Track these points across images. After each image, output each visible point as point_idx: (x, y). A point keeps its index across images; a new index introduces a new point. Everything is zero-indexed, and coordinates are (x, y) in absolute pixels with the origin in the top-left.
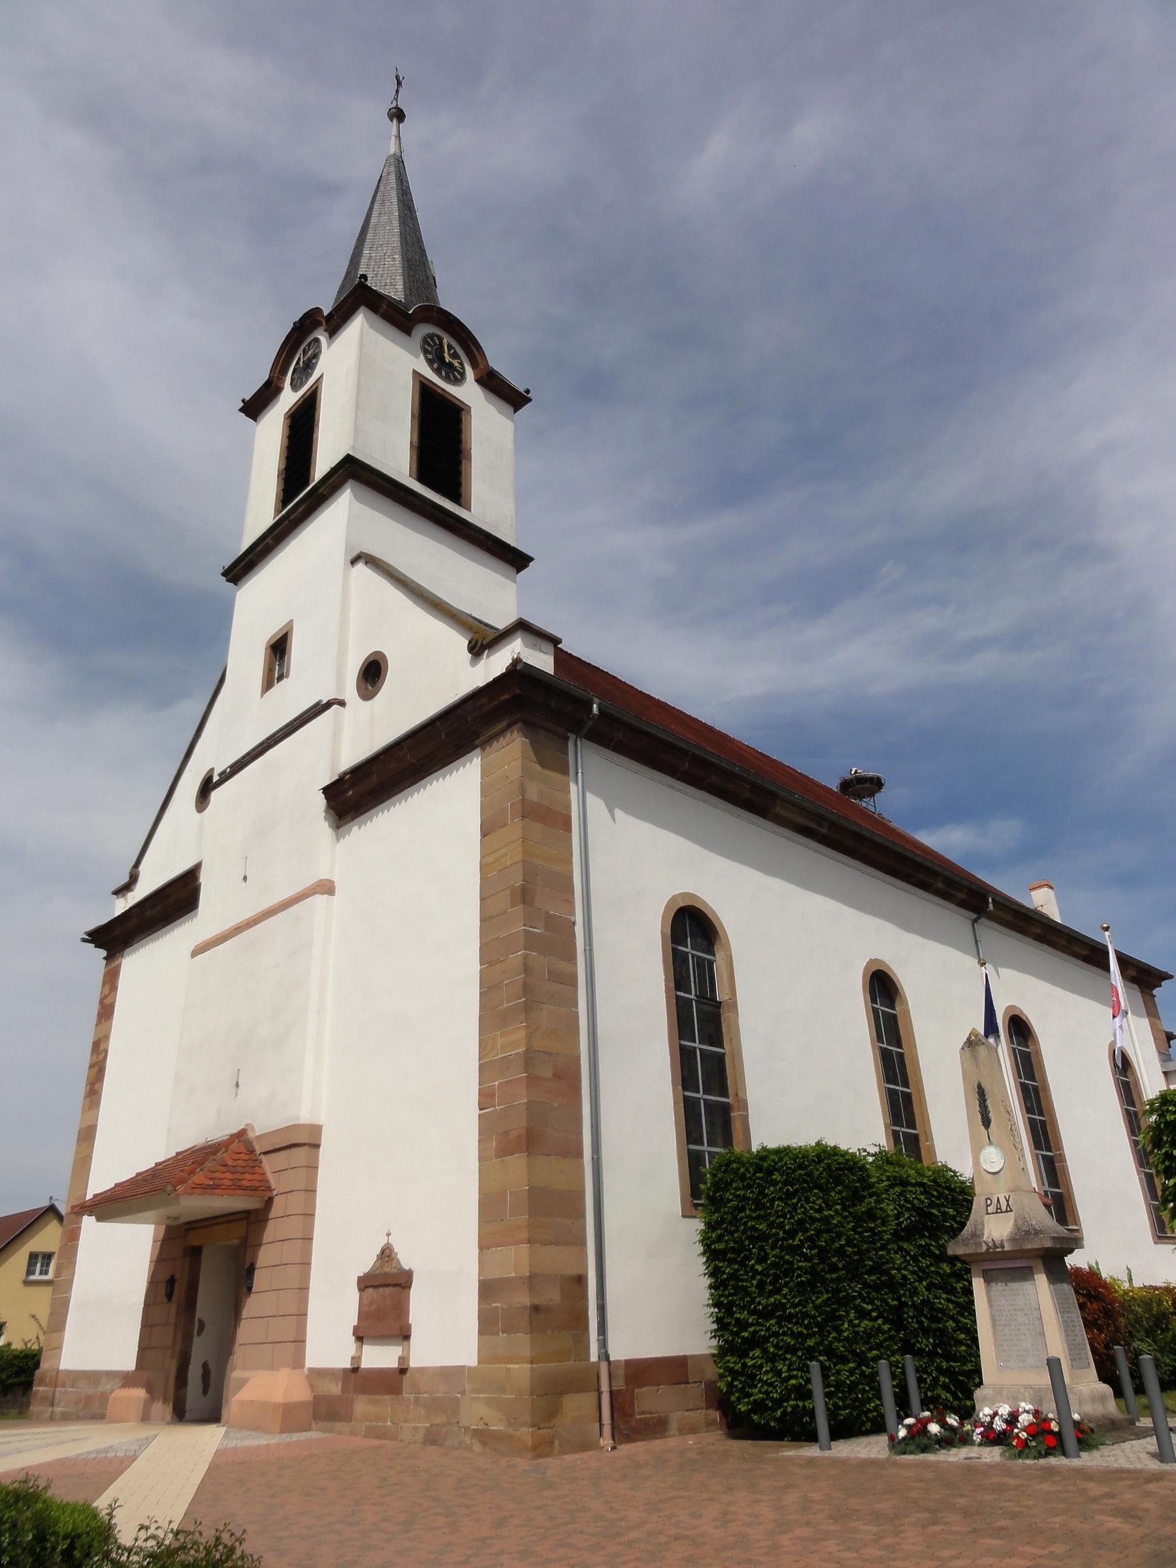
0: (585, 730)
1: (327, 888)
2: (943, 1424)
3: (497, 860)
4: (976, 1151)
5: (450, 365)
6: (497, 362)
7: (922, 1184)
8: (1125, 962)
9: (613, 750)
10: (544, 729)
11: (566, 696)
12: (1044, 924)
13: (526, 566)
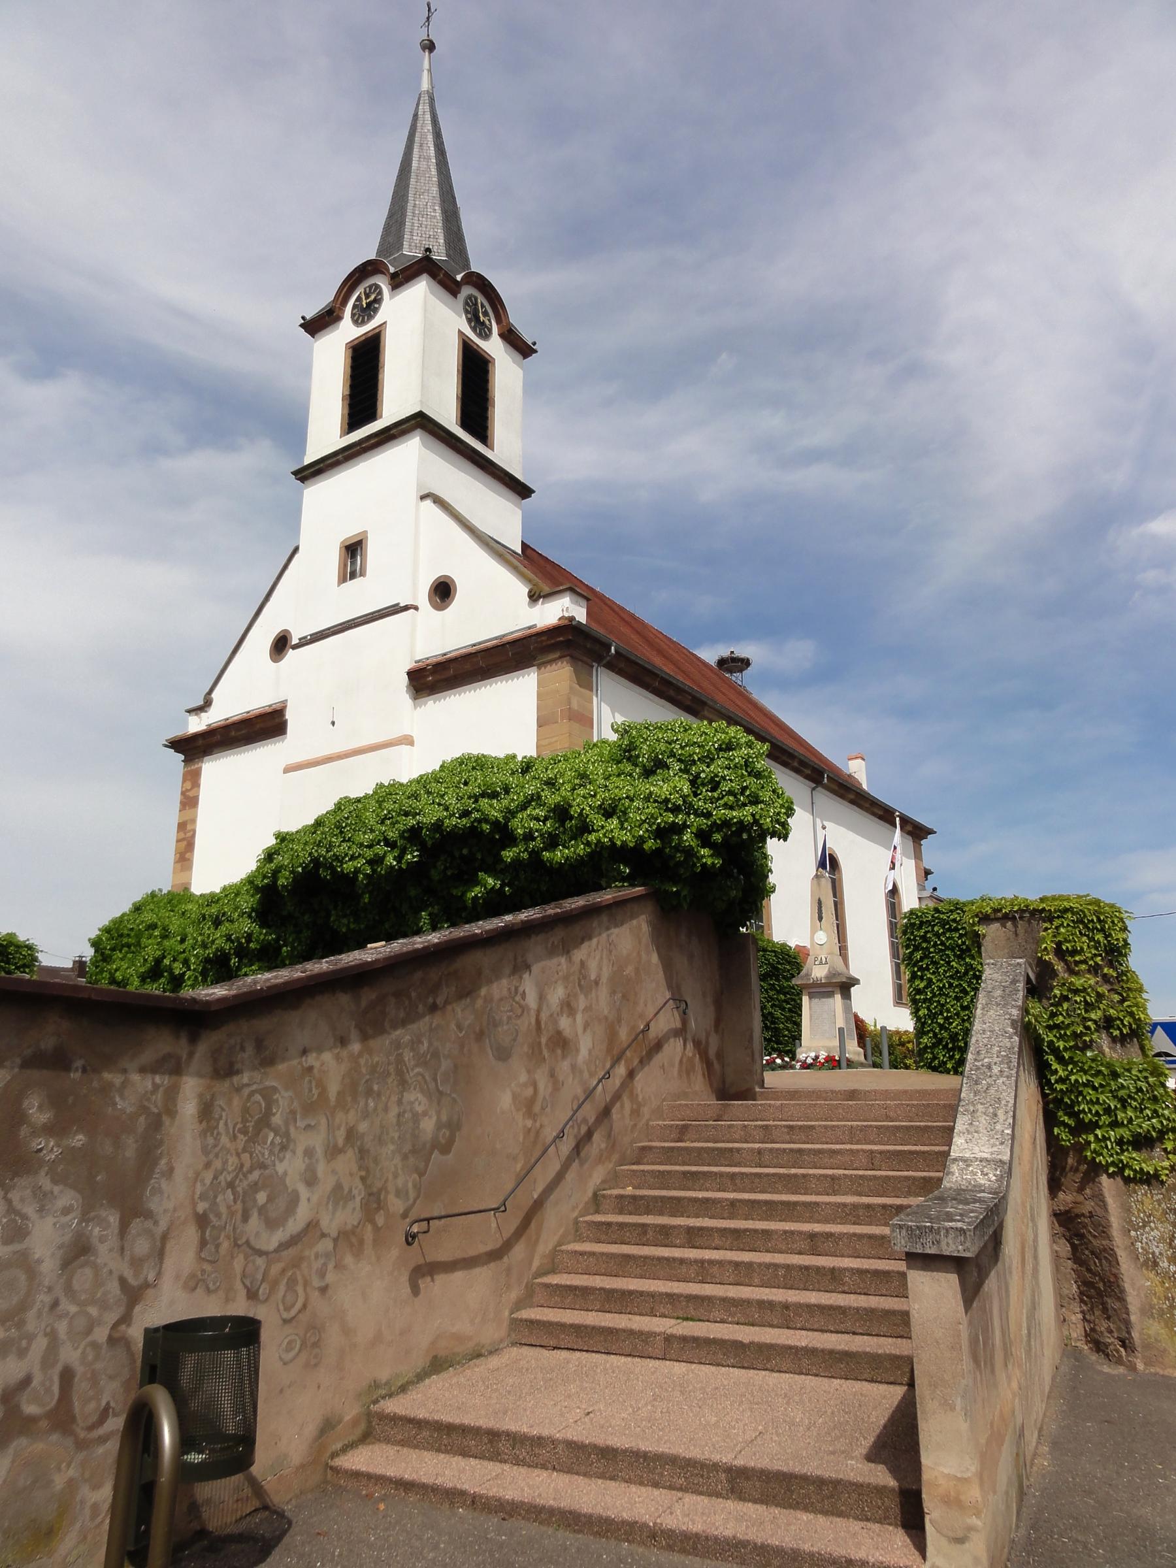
0: (604, 662)
1: (408, 741)
2: (783, 1060)
3: (550, 744)
4: (813, 933)
5: (483, 323)
6: (515, 319)
7: (774, 951)
8: (905, 821)
9: (617, 673)
11: (597, 641)
12: (858, 793)
13: (529, 496)
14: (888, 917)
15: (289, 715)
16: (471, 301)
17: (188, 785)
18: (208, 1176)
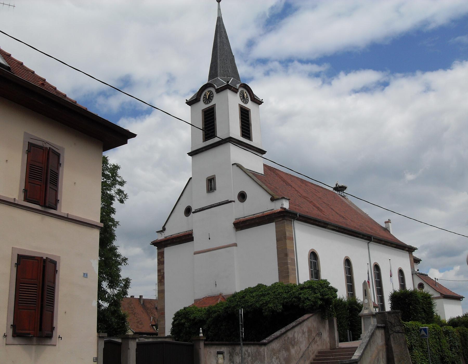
10: (288, 220)
14: (400, 282)
15: (194, 235)
16: (242, 93)
17: (160, 257)
18: (268, 360)
